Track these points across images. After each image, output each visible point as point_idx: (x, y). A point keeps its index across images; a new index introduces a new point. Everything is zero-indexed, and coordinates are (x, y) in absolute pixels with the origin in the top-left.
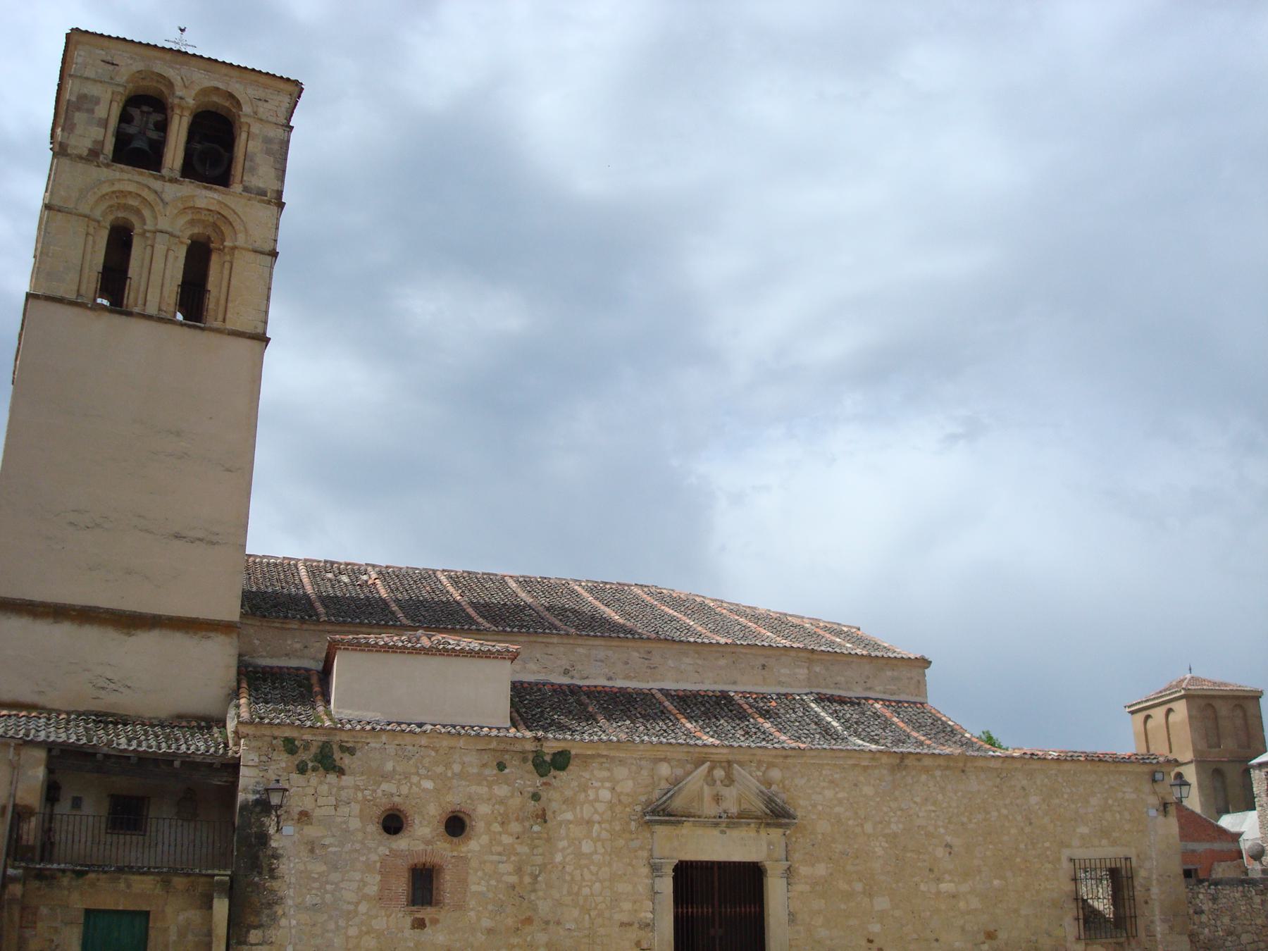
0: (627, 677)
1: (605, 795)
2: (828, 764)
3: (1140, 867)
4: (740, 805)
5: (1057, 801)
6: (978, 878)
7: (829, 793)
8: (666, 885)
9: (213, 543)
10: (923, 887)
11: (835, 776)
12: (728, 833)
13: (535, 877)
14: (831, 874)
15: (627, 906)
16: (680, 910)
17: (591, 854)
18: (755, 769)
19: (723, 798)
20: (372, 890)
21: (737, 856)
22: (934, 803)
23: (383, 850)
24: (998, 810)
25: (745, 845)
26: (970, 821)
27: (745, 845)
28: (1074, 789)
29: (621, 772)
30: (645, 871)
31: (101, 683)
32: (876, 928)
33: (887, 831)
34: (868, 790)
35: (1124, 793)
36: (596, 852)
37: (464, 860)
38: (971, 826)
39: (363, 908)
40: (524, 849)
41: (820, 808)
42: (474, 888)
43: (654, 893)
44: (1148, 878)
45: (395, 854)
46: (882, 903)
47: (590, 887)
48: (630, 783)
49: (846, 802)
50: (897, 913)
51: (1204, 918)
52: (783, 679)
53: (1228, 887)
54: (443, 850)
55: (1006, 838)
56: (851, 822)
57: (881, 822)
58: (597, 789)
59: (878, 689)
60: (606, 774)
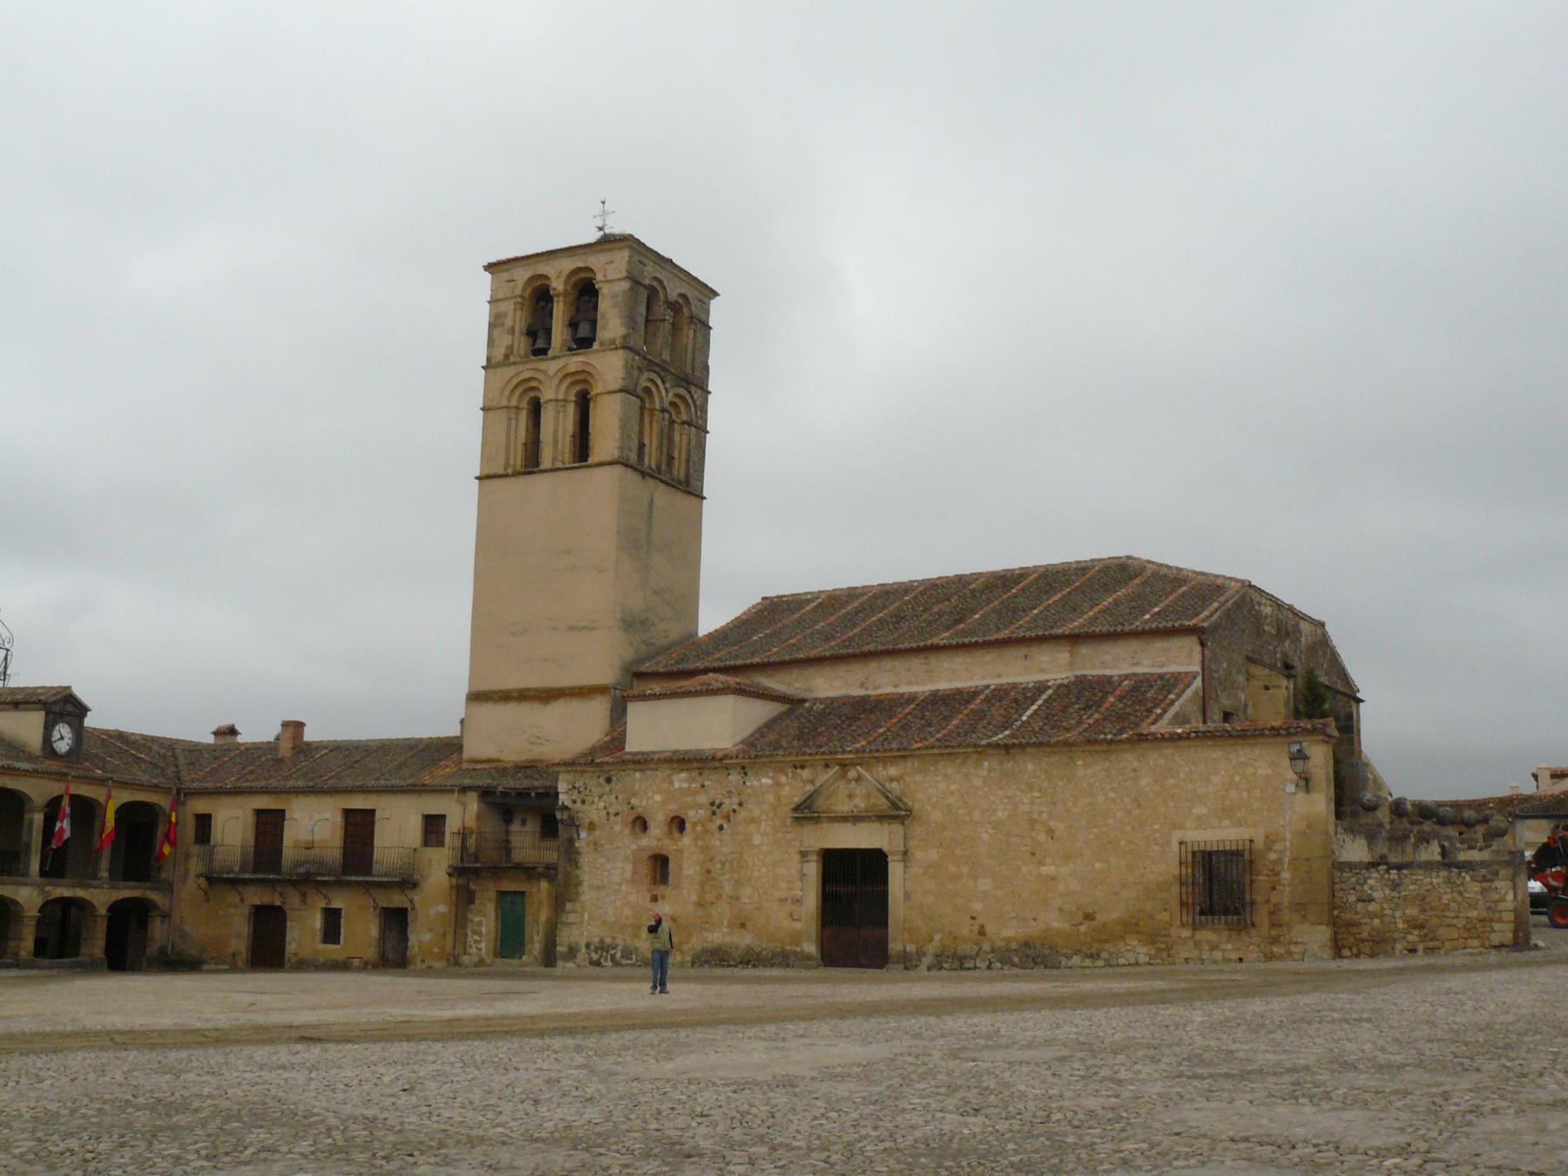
0: (910, 683)
6: (1079, 861)
7: (942, 786)
8: (813, 869)
9: (593, 629)
10: (1024, 869)
17: (760, 845)
20: (628, 875)
23: (634, 847)
24: (1105, 794)
26: (1075, 805)
28: (1193, 768)
30: (797, 857)
32: (978, 906)
37: (680, 851)
38: (1075, 810)
41: (934, 799)
43: (803, 876)
44: (1279, 861)
45: (641, 849)
46: (985, 884)
50: (999, 893)
51: (1372, 907)
53: (1421, 872)
54: (668, 847)
55: (1111, 821)
56: (960, 812)
57: (988, 811)
59: (1145, 662)
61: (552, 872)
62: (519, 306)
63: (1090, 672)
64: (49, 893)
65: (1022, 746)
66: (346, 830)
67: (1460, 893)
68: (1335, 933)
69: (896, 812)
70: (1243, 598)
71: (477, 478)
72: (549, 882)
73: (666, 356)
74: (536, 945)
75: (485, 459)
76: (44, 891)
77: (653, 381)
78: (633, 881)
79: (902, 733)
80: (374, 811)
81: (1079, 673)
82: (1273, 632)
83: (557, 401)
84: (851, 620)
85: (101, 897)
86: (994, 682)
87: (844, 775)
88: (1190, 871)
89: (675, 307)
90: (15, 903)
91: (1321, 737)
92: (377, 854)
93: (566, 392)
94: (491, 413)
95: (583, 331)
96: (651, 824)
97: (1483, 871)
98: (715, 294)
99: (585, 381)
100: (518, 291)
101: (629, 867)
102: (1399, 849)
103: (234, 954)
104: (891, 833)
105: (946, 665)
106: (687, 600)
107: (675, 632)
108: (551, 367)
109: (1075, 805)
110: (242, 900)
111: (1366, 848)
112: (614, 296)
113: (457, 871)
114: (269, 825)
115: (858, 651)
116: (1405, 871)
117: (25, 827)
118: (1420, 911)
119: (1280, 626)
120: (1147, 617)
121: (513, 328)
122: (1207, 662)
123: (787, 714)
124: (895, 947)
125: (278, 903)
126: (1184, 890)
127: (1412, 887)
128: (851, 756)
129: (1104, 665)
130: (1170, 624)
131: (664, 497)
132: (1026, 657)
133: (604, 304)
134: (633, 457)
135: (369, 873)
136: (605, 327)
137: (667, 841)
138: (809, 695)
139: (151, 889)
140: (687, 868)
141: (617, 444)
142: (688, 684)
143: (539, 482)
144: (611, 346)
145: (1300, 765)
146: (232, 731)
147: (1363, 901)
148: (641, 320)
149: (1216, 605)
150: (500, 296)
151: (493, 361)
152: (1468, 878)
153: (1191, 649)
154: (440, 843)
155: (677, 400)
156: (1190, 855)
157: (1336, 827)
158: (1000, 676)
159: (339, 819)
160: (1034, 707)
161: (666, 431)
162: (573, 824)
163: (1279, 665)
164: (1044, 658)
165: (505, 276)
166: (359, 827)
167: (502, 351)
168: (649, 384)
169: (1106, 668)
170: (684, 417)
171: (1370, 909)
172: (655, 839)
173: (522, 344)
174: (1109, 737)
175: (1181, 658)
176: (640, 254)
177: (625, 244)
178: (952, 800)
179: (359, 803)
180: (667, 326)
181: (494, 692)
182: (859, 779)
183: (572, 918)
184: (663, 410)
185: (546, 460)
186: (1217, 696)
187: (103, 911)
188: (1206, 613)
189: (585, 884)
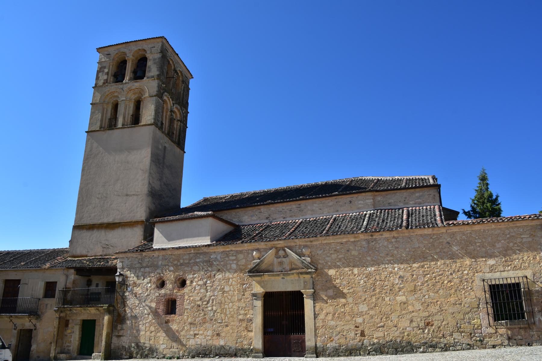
2: (333, 243)
4: (291, 266)
7: (334, 256)
11: (337, 248)
12: (285, 278)
14: (336, 295)
16: (301, 312)
18: (298, 249)
19: (283, 263)
21: (290, 288)
22: (392, 256)
23: (157, 294)
25: (293, 283)
27: (293, 283)
31: (104, 246)
32: (360, 320)
34: (354, 253)
35: (522, 238)
36: (230, 290)
47: (228, 305)
48: (244, 261)
49: (343, 259)
52: (360, 206)
58: (231, 264)
66: (4, 290)
71: (86, 132)
75: (91, 124)
92: (19, 302)
112: (154, 59)
133: (149, 63)
136: (150, 71)
141: (153, 117)
153: (434, 195)
154: (53, 296)
167: (102, 81)
169: (391, 205)
179: (12, 276)
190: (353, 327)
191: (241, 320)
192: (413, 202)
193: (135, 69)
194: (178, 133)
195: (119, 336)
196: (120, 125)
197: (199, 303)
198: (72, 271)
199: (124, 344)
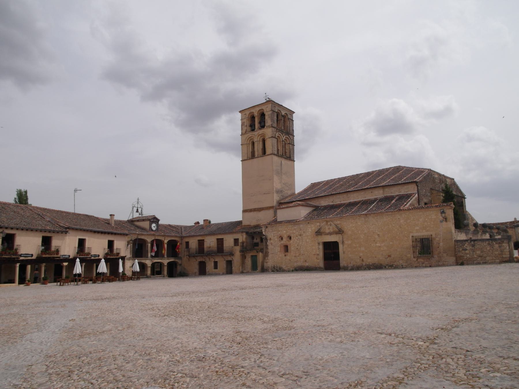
0: (344, 201)
1: (310, 230)
3: (436, 237)
5: (409, 221)
7: (351, 225)
8: (321, 247)
9: (269, 193)
13: (300, 247)
15: (314, 251)
20: (279, 250)
22: (375, 225)
23: (280, 244)
26: (384, 228)
29: (313, 225)
30: (317, 244)
32: (361, 254)
33: (364, 232)
39: (278, 253)
40: (298, 242)
42: (292, 249)
43: (319, 248)
46: (363, 249)
50: (366, 251)
51: (467, 252)
54: (288, 243)
59: (402, 192)
60: (310, 226)
61: (262, 250)
62: (247, 120)
63: (388, 195)
64: (153, 261)
65: (370, 214)
67: (492, 247)
68: (457, 259)
69: (340, 232)
70: (429, 173)
72: (262, 253)
73: (283, 128)
74: (259, 268)
75: (242, 157)
76: (152, 261)
77: (280, 134)
78: (280, 251)
79: (341, 213)
80: (223, 239)
81: (385, 195)
82: (439, 182)
83: (257, 141)
84: (330, 187)
85: (165, 262)
86: (364, 199)
87: (327, 224)
88: (415, 244)
89: (284, 117)
90: (146, 264)
91: (449, 207)
92: (225, 248)
93: (260, 139)
94: (243, 146)
95: (262, 124)
96: (284, 238)
97: (499, 241)
98: (294, 112)
99: (264, 136)
100: (247, 116)
101: (279, 248)
102: (476, 236)
103: (195, 273)
104: (339, 237)
105: (352, 196)
106: (292, 185)
107: (289, 193)
108: (256, 133)
109: (384, 228)
110: (196, 260)
111: (465, 236)
113: (241, 251)
114: (201, 243)
115: (330, 194)
116: (476, 242)
117: (147, 247)
118: (481, 252)
119: (440, 180)
120: (403, 180)
121: (247, 125)
122: (419, 190)
123: (314, 210)
124: (342, 265)
125: (204, 261)
126: (414, 248)
127: (478, 246)
128: (328, 219)
129: (391, 193)
130: (408, 181)
131: (284, 161)
132: (372, 192)
133: (266, 117)
134: (276, 153)
135: (223, 253)
136: (267, 122)
137: (287, 242)
138: (320, 205)
139: (177, 259)
140: (292, 248)
142: (291, 205)
143: (255, 160)
144: (269, 127)
145: (443, 215)
146: (198, 223)
147: (464, 250)
148: (276, 120)
149: (421, 176)
150: (243, 118)
151: (243, 133)
152: (495, 243)
153: (414, 187)
154: (238, 245)
155: (286, 138)
156: (415, 239)
157: (455, 230)
158: (365, 197)
159: (216, 241)
160: (374, 204)
161: (284, 146)
162: (266, 239)
163: (440, 190)
164: (376, 192)
165: (244, 113)
166: (220, 242)
167: (245, 131)
168: (279, 135)
170: (288, 142)
171: (466, 252)
172: (285, 241)
173: (249, 129)
174: (392, 210)
175: (412, 189)
176: (274, 104)
177: (270, 102)
178: (353, 228)
179: (220, 237)
180: (283, 121)
181: (248, 210)
182: (331, 225)
183: (267, 261)
184: (283, 141)
185: (256, 155)
186: (423, 199)
187: (166, 264)
188: (418, 178)
189: (270, 253)
190: (359, 257)
191: (314, 255)
192: (403, 191)
193: (260, 121)
194: (289, 151)
195: (267, 262)
196: (256, 156)
197: (297, 247)
198: (245, 234)
199: (269, 266)
